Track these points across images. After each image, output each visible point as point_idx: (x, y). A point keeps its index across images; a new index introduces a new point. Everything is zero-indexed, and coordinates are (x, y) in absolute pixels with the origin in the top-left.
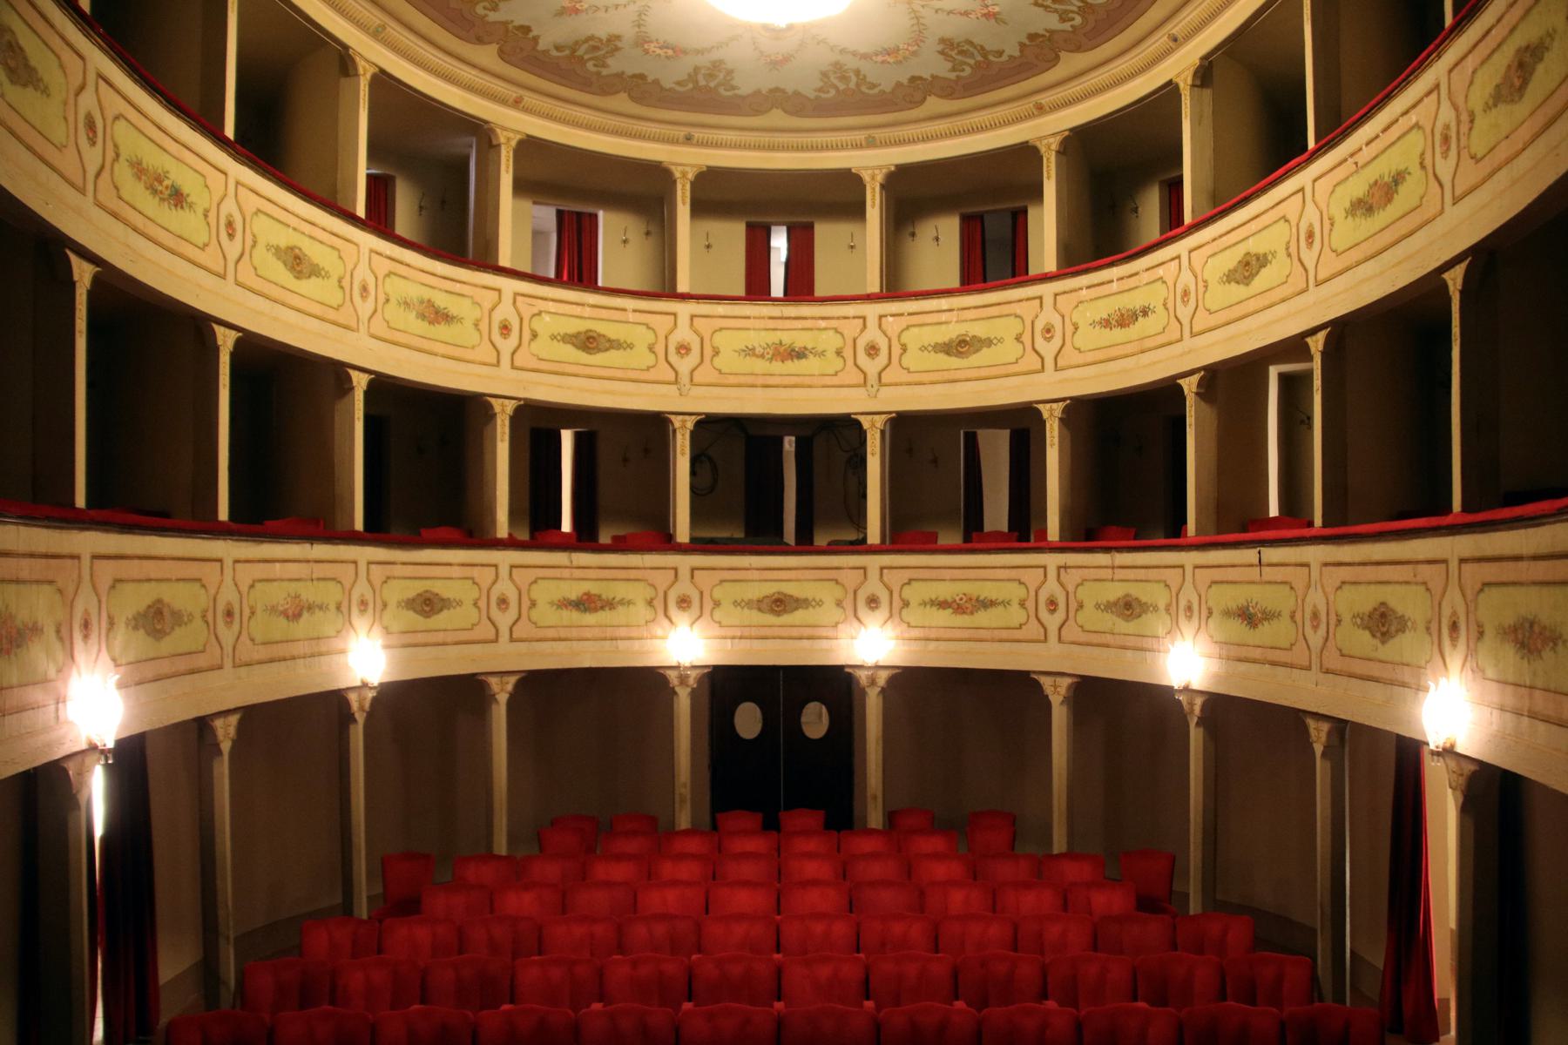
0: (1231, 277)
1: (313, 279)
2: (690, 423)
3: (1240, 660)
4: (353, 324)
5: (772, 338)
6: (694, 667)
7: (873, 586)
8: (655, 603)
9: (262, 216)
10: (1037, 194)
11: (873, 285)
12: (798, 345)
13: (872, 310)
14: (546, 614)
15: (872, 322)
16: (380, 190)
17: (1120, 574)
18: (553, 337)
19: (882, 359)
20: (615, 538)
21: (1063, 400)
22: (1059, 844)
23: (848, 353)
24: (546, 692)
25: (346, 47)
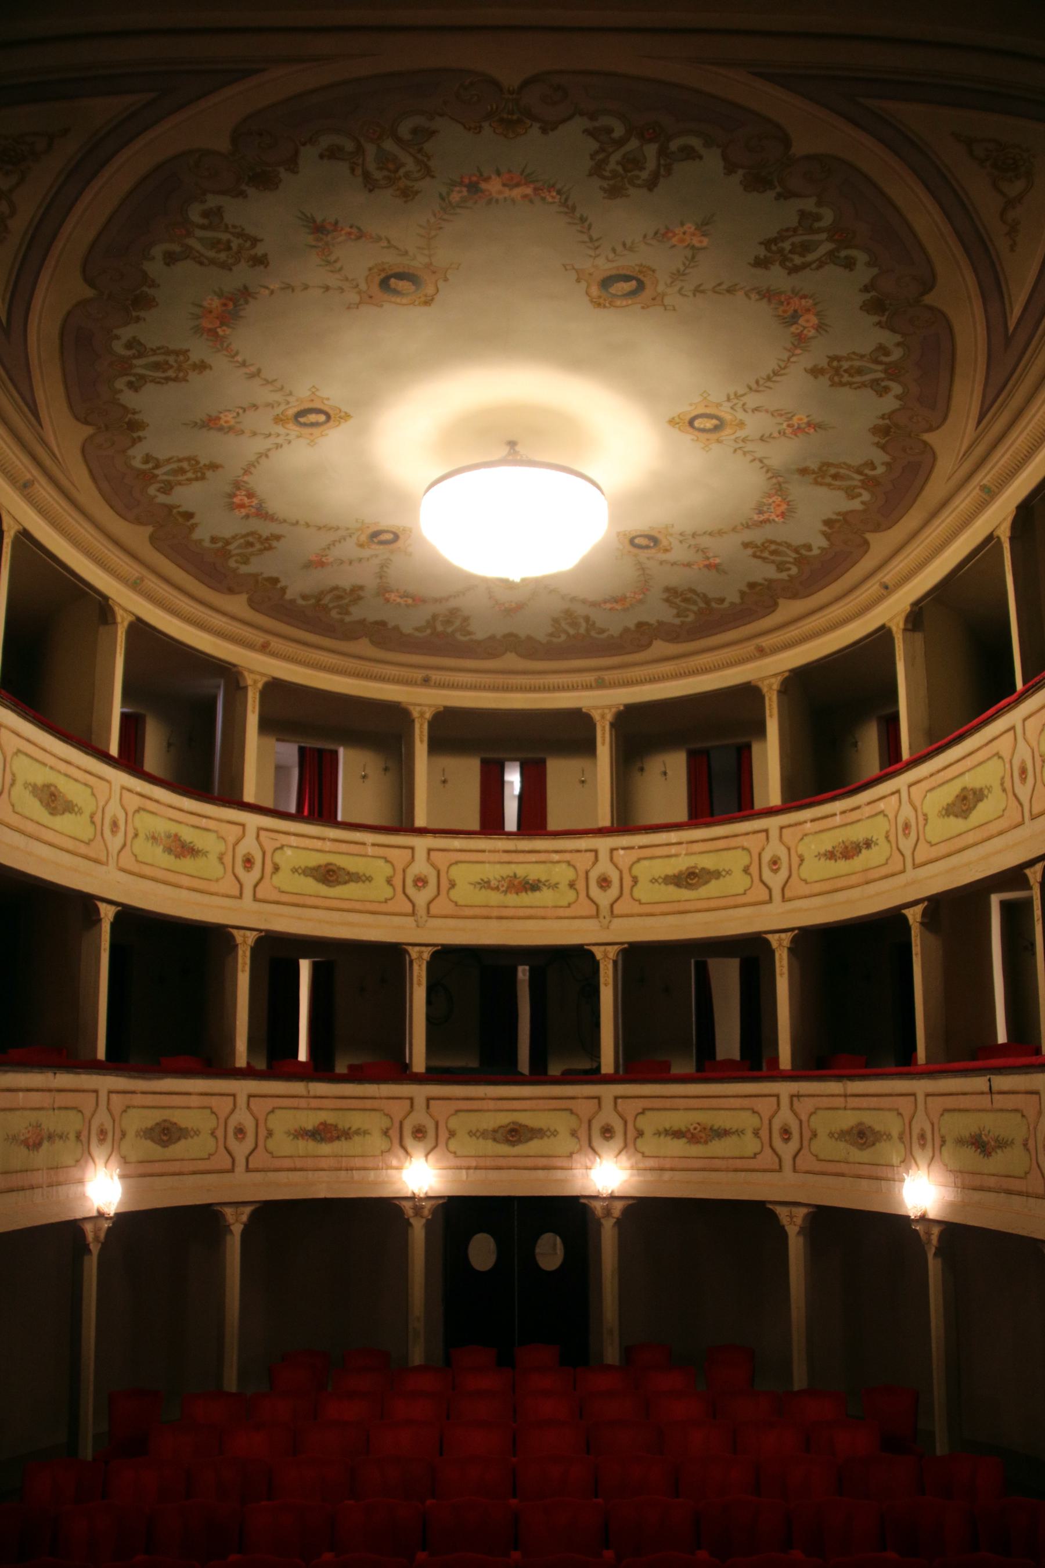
6: (428, 1198)
7: (608, 1116)
8: (391, 1132)
9: (22, 757)
10: (760, 730)
11: (604, 819)
12: (532, 877)
13: (603, 844)
14: (283, 1145)
15: (604, 856)
16: (131, 726)
17: (853, 1102)
18: (295, 870)
19: (614, 891)
20: (351, 1067)
22: (800, 1380)
23: (581, 885)
25: (106, 598)
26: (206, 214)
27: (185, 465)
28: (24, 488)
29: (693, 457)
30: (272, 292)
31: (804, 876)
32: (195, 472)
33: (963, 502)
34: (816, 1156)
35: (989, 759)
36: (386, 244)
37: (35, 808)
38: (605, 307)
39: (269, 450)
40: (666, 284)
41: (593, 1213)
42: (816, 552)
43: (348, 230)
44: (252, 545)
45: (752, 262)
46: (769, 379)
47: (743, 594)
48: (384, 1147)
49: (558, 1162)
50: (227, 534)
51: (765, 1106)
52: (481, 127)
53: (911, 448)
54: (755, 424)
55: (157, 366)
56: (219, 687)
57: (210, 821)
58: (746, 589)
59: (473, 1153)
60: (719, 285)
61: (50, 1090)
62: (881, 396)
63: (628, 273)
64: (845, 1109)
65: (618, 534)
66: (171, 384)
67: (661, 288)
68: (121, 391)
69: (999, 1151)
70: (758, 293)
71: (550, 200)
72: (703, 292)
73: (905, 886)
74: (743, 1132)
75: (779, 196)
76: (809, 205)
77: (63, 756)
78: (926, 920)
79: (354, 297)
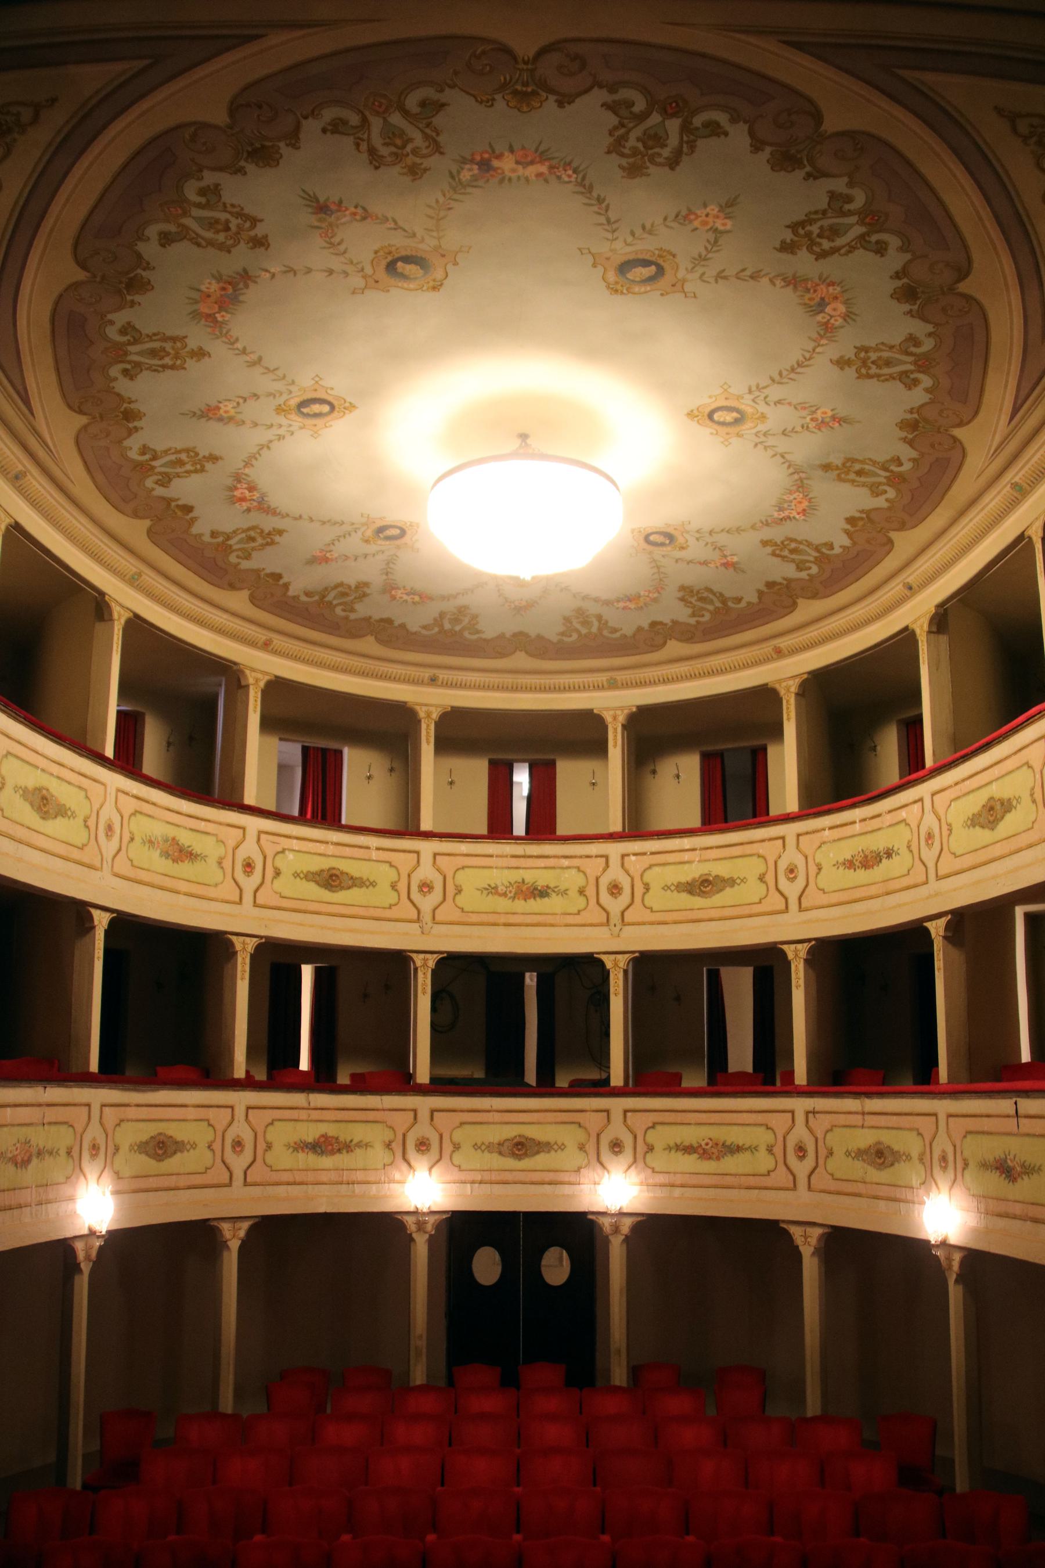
0: (974, 821)
1: (59, 818)
2: (432, 961)
3: (1000, 1215)
4: (97, 863)
5: (515, 876)
7: (617, 1129)
8: (394, 1145)
9: (10, 758)
10: (776, 732)
11: (616, 824)
12: (541, 883)
14: (282, 1158)
16: (129, 727)
17: (870, 1120)
18: (296, 875)
19: (625, 898)
20: (353, 1076)
21: (809, 940)
22: (813, 1407)
23: (591, 891)
24: (281, 1238)
25: (102, 594)
26: (202, 192)
27: (183, 456)
28: (16, 480)
29: (711, 451)
30: (273, 276)
31: (821, 886)
32: (194, 464)
33: (993, 501)
34: (832, 1175)
35: (1018, 768)
36: (393, 226)
37: (28, 814)
38: (622, 293)
39: (271, 441)
40: (687, 269)
41: (601, 1229)
42: (837, 550)
43: (353, 209)
44: (253, 539)
45: (778, 246)
46: (793, 370)
47: (761, 594)
48: (387, 1160)
49: (565, 1177)
50: (228, 528)
51: (780, 1122)
52: (493, 99)
53: (940, 444)
54: (777, 417)
55: (153, 353)
56: (220, 685)
57: (208, 824)
58: (765, 589)
59: (478, 1166)
60: (743, 270)
61: (40, 1105)
62: (910, 389)
63: (647, 257)
64: (863, 1127)
65: (633, 531)
66: (169, 372)
67: (681, 274)
68: (116, 379)
69: (1025, 1177)
70: (784, 280)
71: (566, 179)
72: (725, 278)
73: (927, 898)
74: (756, 1148)
75: (809, 175)
76: (839, 185)
77: (55, 758)
78: (949, 934)
79: (359, 282)
